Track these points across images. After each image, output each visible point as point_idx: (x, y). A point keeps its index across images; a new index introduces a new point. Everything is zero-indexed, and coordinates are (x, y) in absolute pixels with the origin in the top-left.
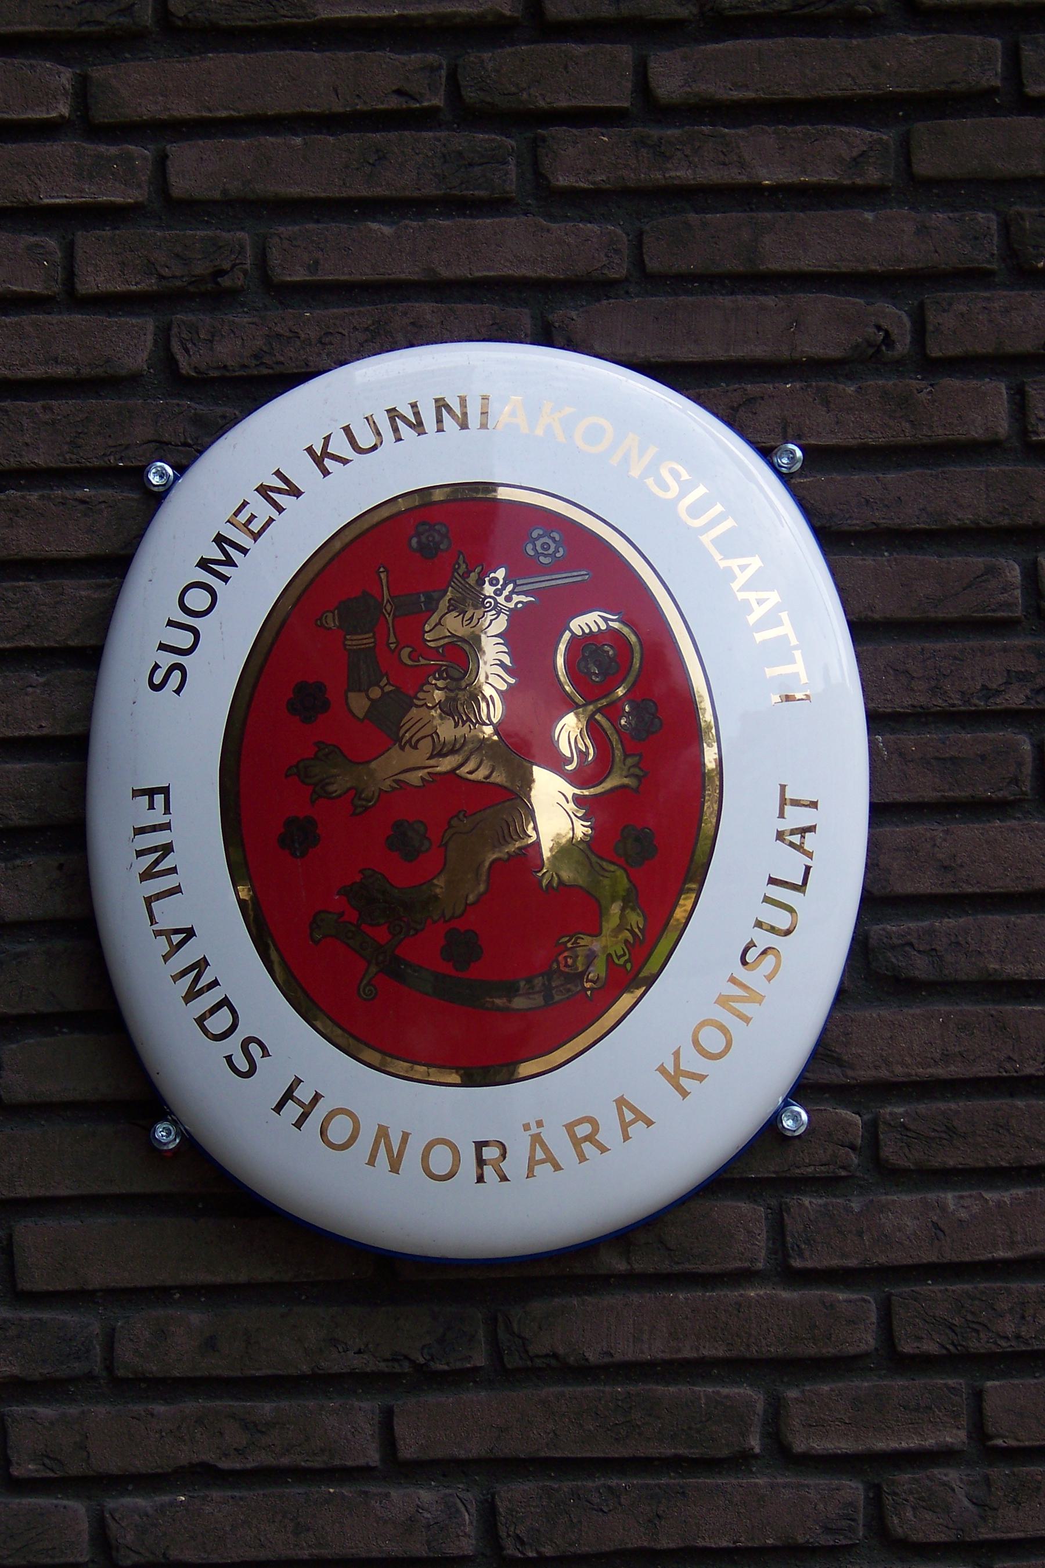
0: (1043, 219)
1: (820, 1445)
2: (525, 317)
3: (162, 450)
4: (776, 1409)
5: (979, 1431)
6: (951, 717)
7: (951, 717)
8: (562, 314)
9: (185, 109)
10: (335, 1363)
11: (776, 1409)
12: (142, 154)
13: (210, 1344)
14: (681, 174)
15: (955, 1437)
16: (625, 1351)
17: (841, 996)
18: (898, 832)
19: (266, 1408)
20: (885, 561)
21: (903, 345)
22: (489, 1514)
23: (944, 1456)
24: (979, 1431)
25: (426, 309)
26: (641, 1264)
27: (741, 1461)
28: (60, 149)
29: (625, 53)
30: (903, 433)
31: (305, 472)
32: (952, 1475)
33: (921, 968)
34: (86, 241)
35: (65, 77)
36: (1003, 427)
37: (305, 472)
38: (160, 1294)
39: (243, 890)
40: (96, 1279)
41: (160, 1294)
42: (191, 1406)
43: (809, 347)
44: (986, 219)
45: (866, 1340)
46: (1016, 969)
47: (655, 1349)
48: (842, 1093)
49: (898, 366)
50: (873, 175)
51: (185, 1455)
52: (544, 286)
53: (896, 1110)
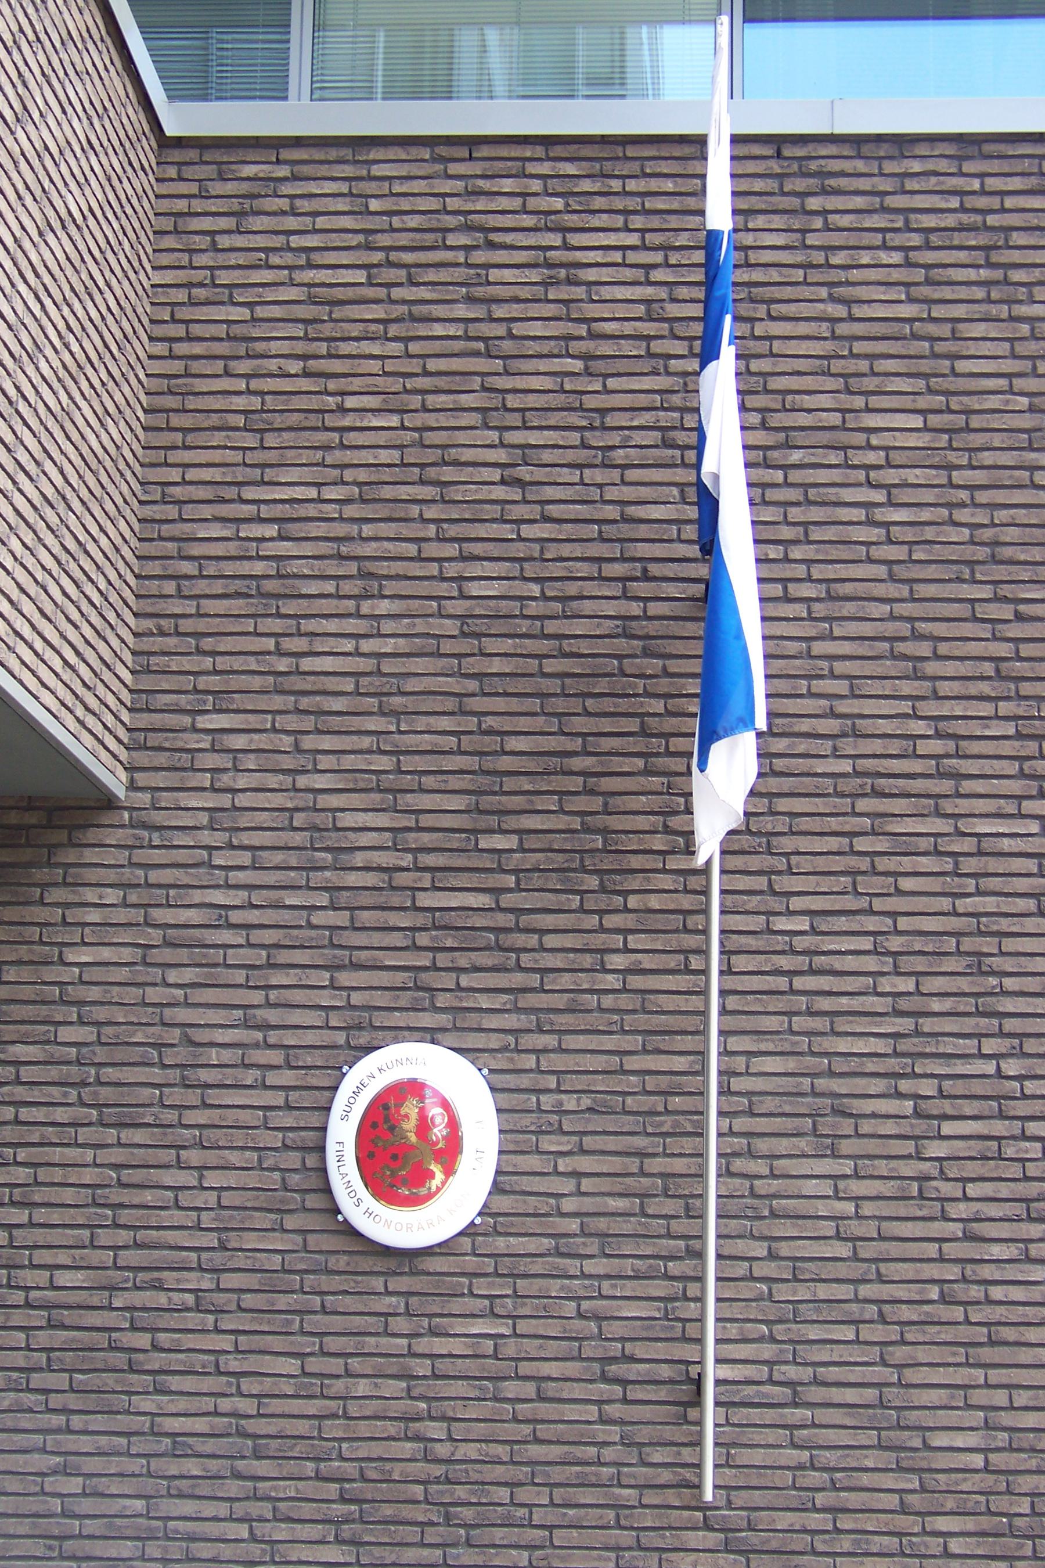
0: (4, 1262)
1: (480, 1292)
2: (429, 1037)
3: (346, 1063)
4: (471, 1284)
5: (515, 1291)
6: (518, 1131)
7: (518, 1131)
8: (439, 1036)
9: (355, 985)
10: (375, 1269)
11: (471, 1284)
12: (345, 994)
13: (348, 1264)
14: (465, 1005)
15: (510, 1292)
16: (439, 1270)
17: (490, 1193)
18: (504, 1157)
19: (360, 1278)
20: (505, 1095)
21: (513, 1046)
22: (407, 1304)
23: (506, 1296)
24: (515, 1291)
25: (406, 1033)
26: (443, 1251)
27: (463, 1295)
28: (325, 992)
29: (454, 975)
30: (511, 1067)
31: (376, 1073)
32: (508, 1300)
33: (508, 1188)
34: (331, 1014)
35: (328, 975)
36: (534, 1066)
37: (376, 1073)
38: (337, 1252)
39: (531, 1022)
40: (324, 1248)
41: (337, 1252)
42: (343, 1277)
43: (492, 1046)
44: (534, 1018)
45: (491, 1270)
46: (528, 1189)
47: (445, 1270)
48: (489, 1215)
49: (512, 1051)
50: (508, 1007)
51: (342, 1288)
52: (516, 1030)
53: (501, 1219)
